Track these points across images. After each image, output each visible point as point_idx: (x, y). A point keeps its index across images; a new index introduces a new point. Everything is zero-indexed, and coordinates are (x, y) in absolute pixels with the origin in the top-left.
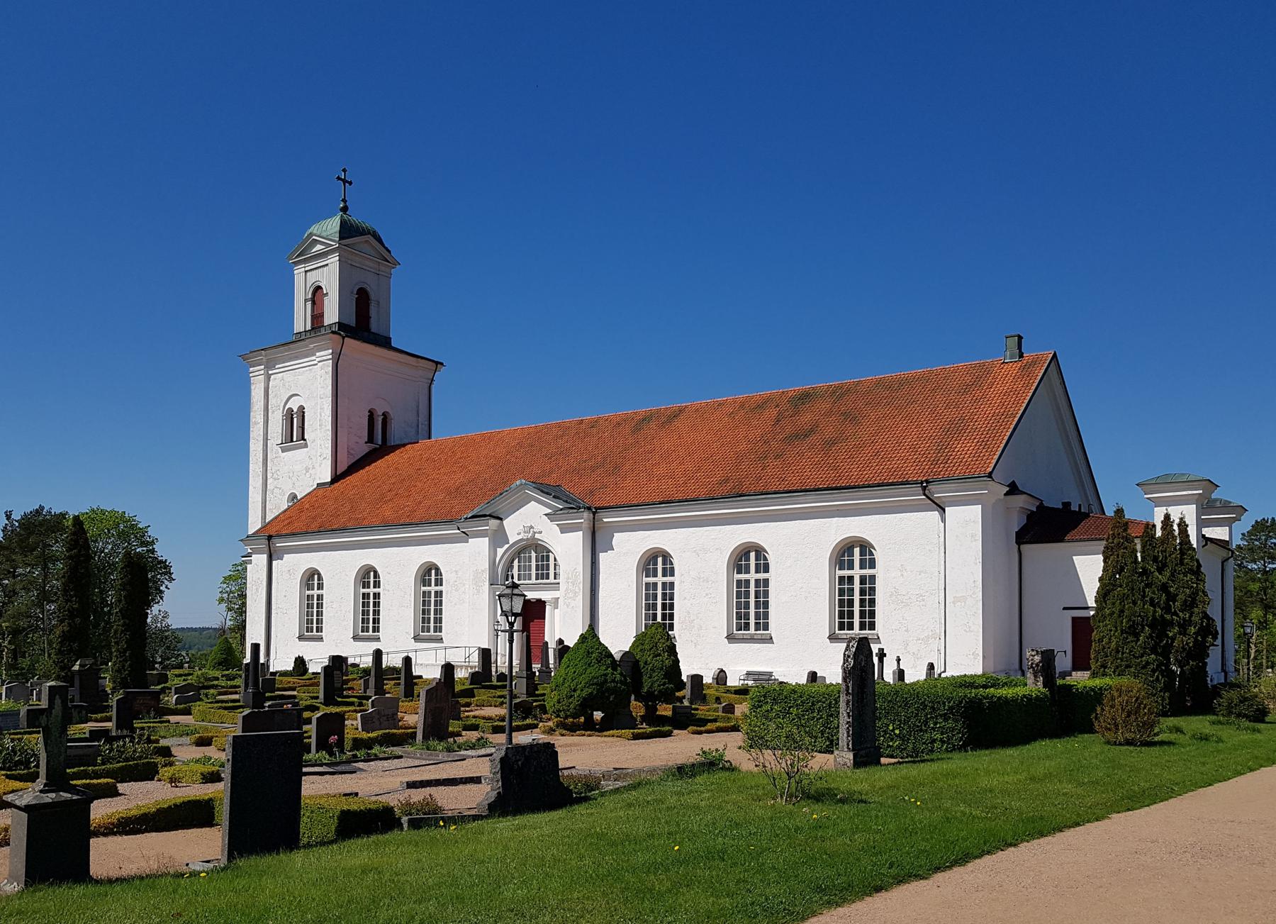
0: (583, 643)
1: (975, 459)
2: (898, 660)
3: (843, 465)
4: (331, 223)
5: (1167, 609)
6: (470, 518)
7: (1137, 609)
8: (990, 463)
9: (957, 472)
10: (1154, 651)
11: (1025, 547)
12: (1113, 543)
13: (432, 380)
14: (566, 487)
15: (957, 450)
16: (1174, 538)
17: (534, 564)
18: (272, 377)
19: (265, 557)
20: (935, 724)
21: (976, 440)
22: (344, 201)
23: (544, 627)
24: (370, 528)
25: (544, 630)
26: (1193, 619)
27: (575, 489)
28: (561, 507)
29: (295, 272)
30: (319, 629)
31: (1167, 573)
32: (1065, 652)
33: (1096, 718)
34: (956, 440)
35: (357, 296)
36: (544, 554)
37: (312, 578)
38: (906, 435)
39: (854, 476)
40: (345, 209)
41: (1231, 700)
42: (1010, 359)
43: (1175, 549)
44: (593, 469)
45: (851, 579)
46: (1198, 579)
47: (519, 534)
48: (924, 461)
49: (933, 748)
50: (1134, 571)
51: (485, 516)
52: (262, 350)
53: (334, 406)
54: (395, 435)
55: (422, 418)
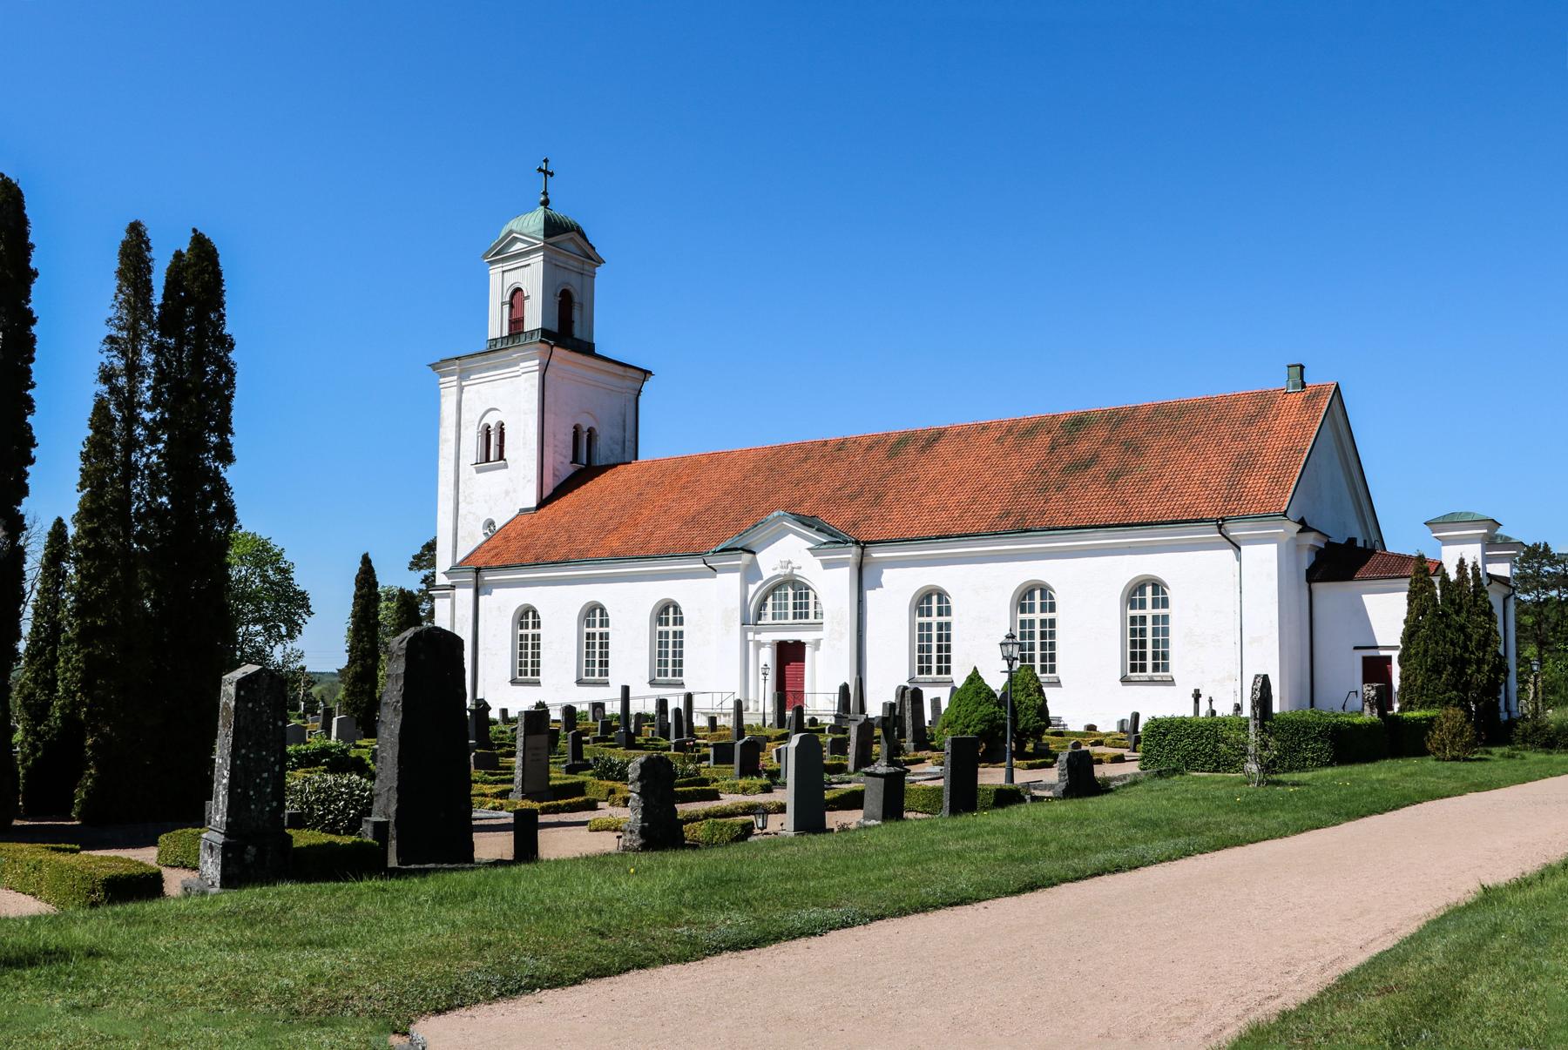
0: (970, 684)
1: (1268, 496)
2: (1211, 701)
3: (1132, 500)
4: (533, 219)
5: (1465, 648)
6: (719, 551)
7: (1439, 649)
8: (1284, 501)
9: (1252, 509)
10: (1455, 687)
11: (1318, 587)
12: (1416, 587)
13: (640, 391)
14: (824, 518)
15: (1248, 486)
16: (1468, 581)
17: (791, 601)
18: (466, 388)
19: (470, 592)
20: (1307, 745)
21: (1267, 477)
22: (545, 193)
23: (803, 671)
24: (597, 561)
25: (803, 674)
26: (1486, 657)
27: (839, 519)
28: (825, 541)
29: (491, 272)
30: (536, 673)
31: (1464, 615)
32: (1356, 692)
33: (1429, 740)
34: (1247, 476)
35: (560, 299)
36: (802, 590)
37: (527, 616)
38: (1195, 469)
39: (1146, 511)
40: (545, 203)
41: (1525, 729)
42: (1294, 388)
43: (1469, 591)
44: (852, 498)
45: (1143, 619)
46: (1490, 620)
47: (775, 569)
48: (1217, 497)
49: (1305, 764)
50: (1435, 614)
51: (736, 549)
52: (456, 359)
53: (541, 420)
54: (602, 454)
55: (629, 434)
